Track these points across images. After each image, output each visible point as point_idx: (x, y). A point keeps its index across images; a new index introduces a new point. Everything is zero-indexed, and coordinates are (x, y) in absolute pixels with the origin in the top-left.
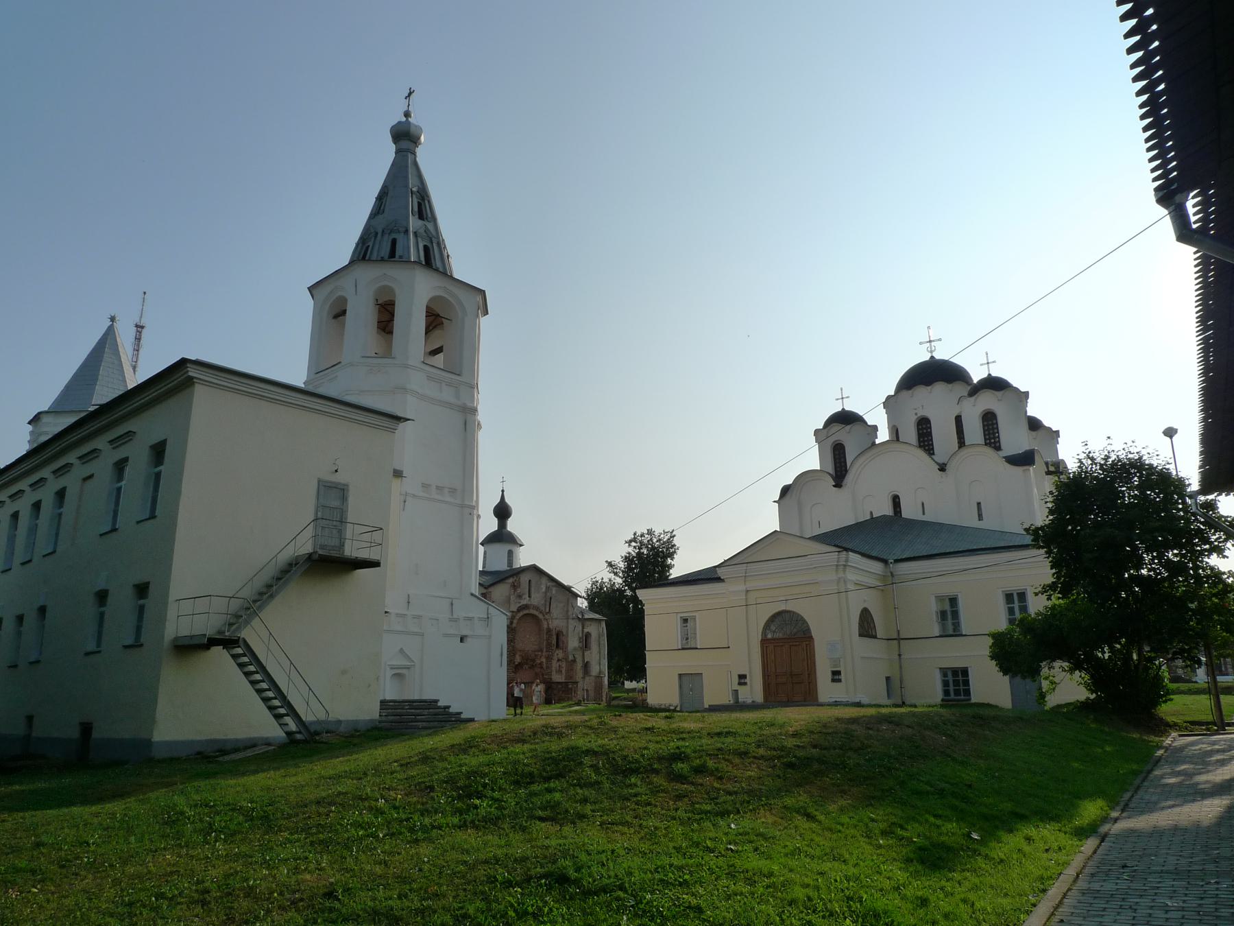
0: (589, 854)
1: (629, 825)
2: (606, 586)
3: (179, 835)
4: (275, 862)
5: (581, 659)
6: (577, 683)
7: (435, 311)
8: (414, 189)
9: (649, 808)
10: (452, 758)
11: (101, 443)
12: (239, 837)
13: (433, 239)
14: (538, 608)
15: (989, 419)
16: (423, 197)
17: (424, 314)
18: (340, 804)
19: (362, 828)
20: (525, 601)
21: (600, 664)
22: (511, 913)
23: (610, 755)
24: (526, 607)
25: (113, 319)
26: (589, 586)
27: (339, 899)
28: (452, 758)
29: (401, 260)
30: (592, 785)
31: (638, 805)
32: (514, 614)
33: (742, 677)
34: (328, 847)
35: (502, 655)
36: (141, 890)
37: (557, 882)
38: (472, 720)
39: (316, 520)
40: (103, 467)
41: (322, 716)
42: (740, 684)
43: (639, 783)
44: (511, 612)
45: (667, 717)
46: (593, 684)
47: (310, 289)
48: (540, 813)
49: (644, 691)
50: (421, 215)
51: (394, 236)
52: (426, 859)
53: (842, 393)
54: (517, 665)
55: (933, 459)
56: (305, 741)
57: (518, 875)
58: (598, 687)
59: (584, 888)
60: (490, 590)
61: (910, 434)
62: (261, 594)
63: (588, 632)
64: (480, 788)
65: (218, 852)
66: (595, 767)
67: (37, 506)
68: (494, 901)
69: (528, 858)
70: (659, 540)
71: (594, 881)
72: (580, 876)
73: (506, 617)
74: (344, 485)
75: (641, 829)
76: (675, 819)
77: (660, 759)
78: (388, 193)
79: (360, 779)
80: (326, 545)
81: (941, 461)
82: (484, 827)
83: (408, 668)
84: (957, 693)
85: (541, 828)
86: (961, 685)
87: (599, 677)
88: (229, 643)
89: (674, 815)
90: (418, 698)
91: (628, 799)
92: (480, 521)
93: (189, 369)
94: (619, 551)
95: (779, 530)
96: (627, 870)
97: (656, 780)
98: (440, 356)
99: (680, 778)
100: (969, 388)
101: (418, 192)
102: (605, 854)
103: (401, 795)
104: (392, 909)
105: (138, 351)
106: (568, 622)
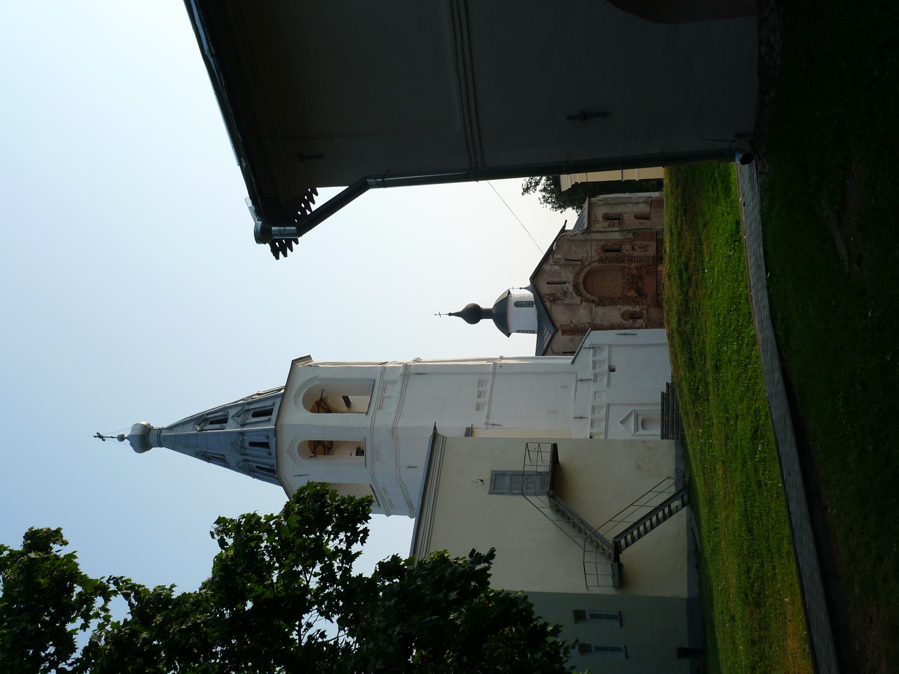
8: (198, 429)
16: (203, 420)
20: (570, 287)
24: (576, 287)
26: (549, 206)
32: (584, 299)
35: (626, 334)
44: (581, 303)
50: (224, 421)
51: (247, 445)
60: (558, 324)
63: (603, 217)
74: (492, 474)
78: (204, 452)
80: (541, 486)
83: (637, 415)
88: (617, 549)
90: (660, 407)
92: (505, 356)
101: (199, 425)
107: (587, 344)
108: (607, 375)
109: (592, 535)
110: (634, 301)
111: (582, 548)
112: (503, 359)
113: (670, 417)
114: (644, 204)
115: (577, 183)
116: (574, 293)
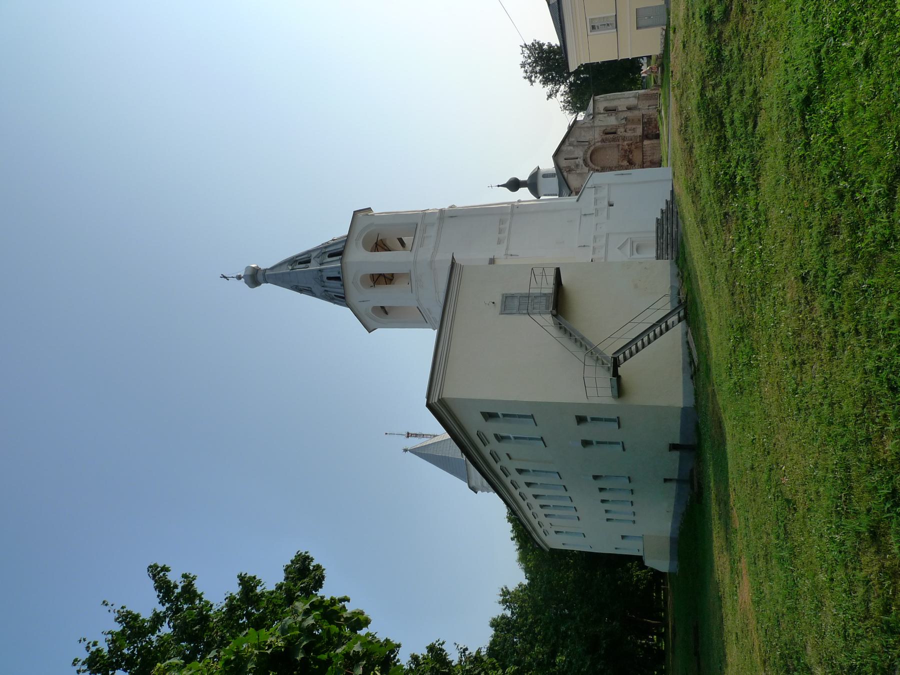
0: (788, 81)
1: (764, 52)
2: (567, 98)
3: (751, 384)
4: (776, 319)
5: (625, 113)
6: (643, 115)
7: (374, 246)
8: (290, 268)
9: (751, 37)
10: (703, 202)
11: (486, 451)
12: (755, 345)
13: (323, 252)
14: (585, 151)
18: (734, 279)
19: (754, 261)
20: (580, 161)
21: (628, 98)
22: (832, 140)
23: (705, 75)
25: (406, 450)
26: (568, 112)
27: (808, 271)
28: (703, 202)
29: (341, 273)
30: (729, 88)
31: (748, 46)
32: (590, 169)
34: (767, 284)
36: (789, 404)
37: (808, 106)
38: (672, 192)
40: (502, 449)
41: (668, 299)
43: (729, 48)
44: (589, 172)
45: (674, 32)
46: (644, 102)
47: (370, 332)
48: (750, 127)
49: (649, 57)
50: (308, 262)
51: (325, 279)
52: (782, 212)
54: (629, 164)
56: (685, 309)
57: (801, 138)
58: (647, 97)
59: (815, 82)
60: (572, 188)
62: (581, 345)
63: (604, 110)
64: (728, 177)
65: (765, 358)
66: (714, 88)
67: (529, 484)
68: (820, 155)
69: (787, 132)
70: (529, 57)
71: (810, 75)
72: (805, 88)
73: (594, 174)
75: (769, 40)
76: (761, 12)
77: (710, 32)
79: (716, 267)
82: (759, 171)
83: (632, 242)
85: (763, 125)
87: (638, 98)
88: (616, 364)
89: (757, 13)
91: (742, 56)
92: (522, 200)
93: (433, 402)
94: (540, 89)
96: (803, 48)
97: (726, 34)
98: (405, 239)
99: (727, 13)
102: (788, 69)
103: (730, 236)
104: (820, 232)
105: (424, 435)
106: (596, 127)
107: (589, 185)
108: (606, 210)
109: (592, 351)
112: (520, 202)
113: (664, 239)
114: (633, 98)
116: (583, 165)
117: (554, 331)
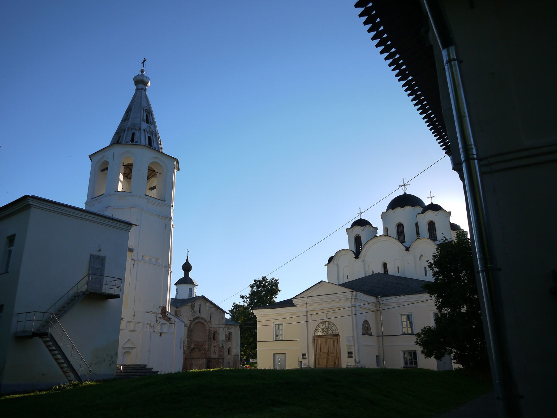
6: (224, 358)
15: (432, 226)
17: (147, 170)
20: (197, 316)
24: (198, 318)
33: (304, 355)
39: (89, 274)
42: (303, 358)
49: (256, 363)
50: (147, 122)
51: (133, 131)
53: (360, 210)
55: (403, 245)
61: (393, 231)
81: (407, 246)
84: (411, 363)
86: (413, 360)
93: (29, 200)
95: (326, 279)
100: (422, 209)
110: (189, 347)
111: (46, 311)
115: (256, 318)
117: (71, 293)
